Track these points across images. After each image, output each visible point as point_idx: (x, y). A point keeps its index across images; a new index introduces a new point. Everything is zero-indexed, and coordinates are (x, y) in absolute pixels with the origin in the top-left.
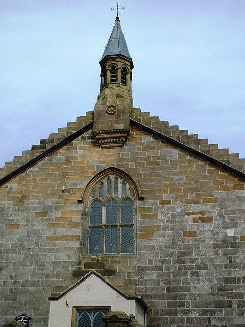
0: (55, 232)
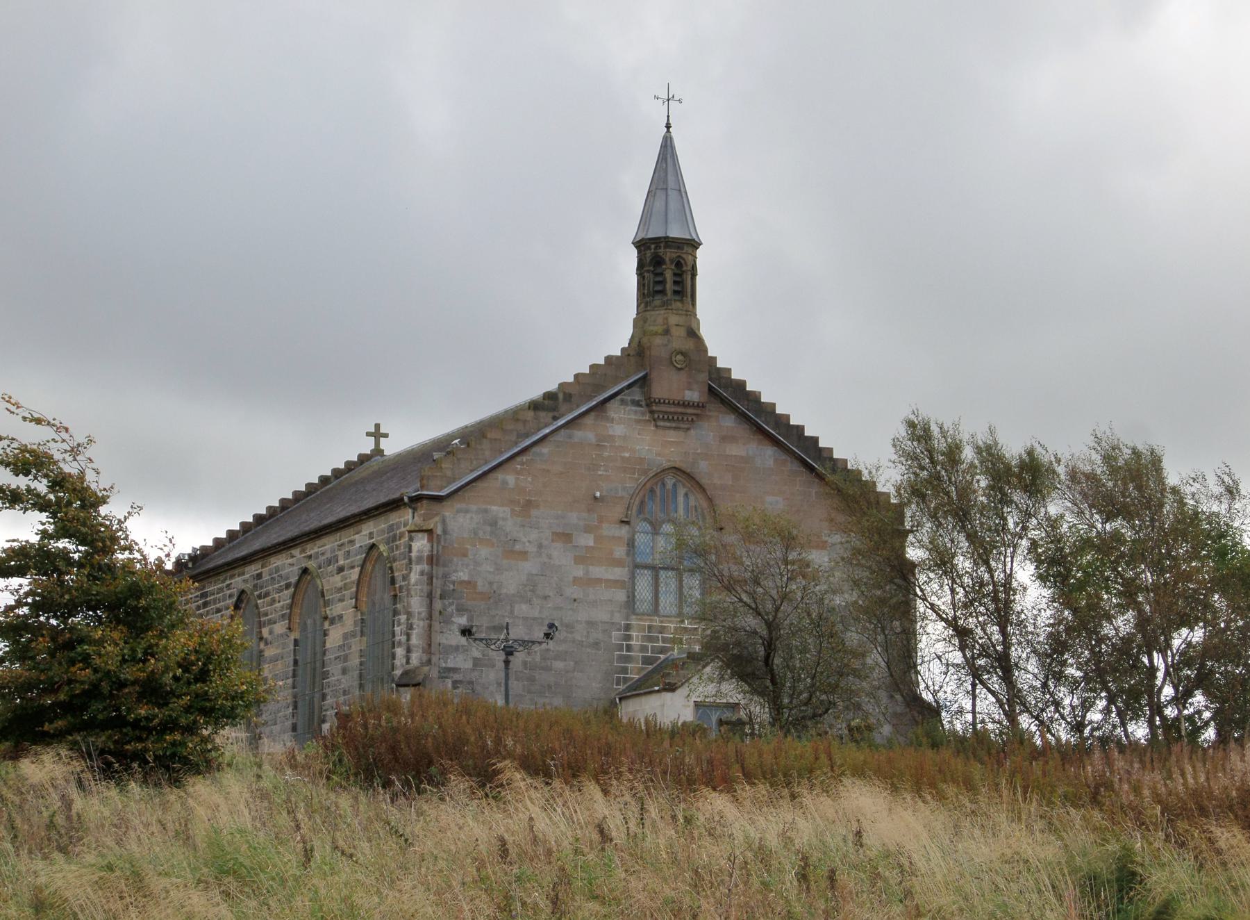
0: (587, 572)
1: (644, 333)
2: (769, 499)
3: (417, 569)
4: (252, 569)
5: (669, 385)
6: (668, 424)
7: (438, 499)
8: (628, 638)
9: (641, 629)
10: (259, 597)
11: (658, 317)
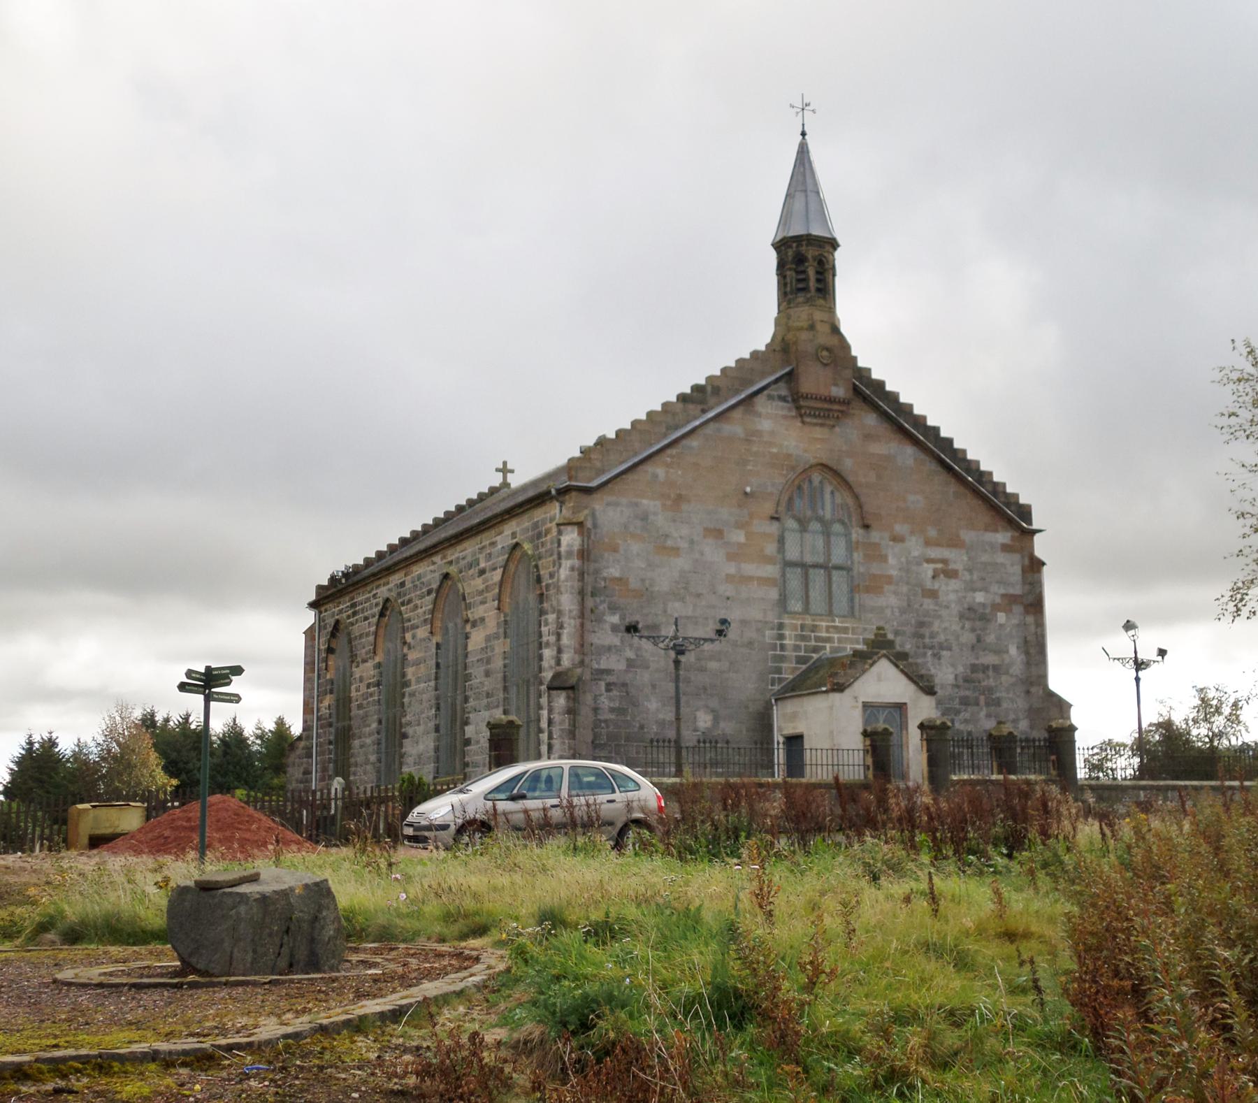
1: (789, 329)
2: (911, 498)
3: (566, 564)
4: (396, 579)
5: (815, 380)
6: (815, 421)
7: (587, 491)
8: (781, 637)
9: (794, 628)
10: (403, 604)
11: (802, 314)
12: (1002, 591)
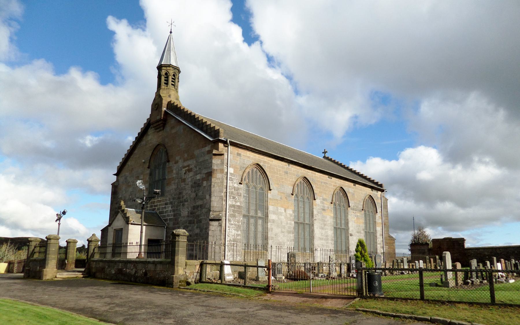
12: (206, 172)
